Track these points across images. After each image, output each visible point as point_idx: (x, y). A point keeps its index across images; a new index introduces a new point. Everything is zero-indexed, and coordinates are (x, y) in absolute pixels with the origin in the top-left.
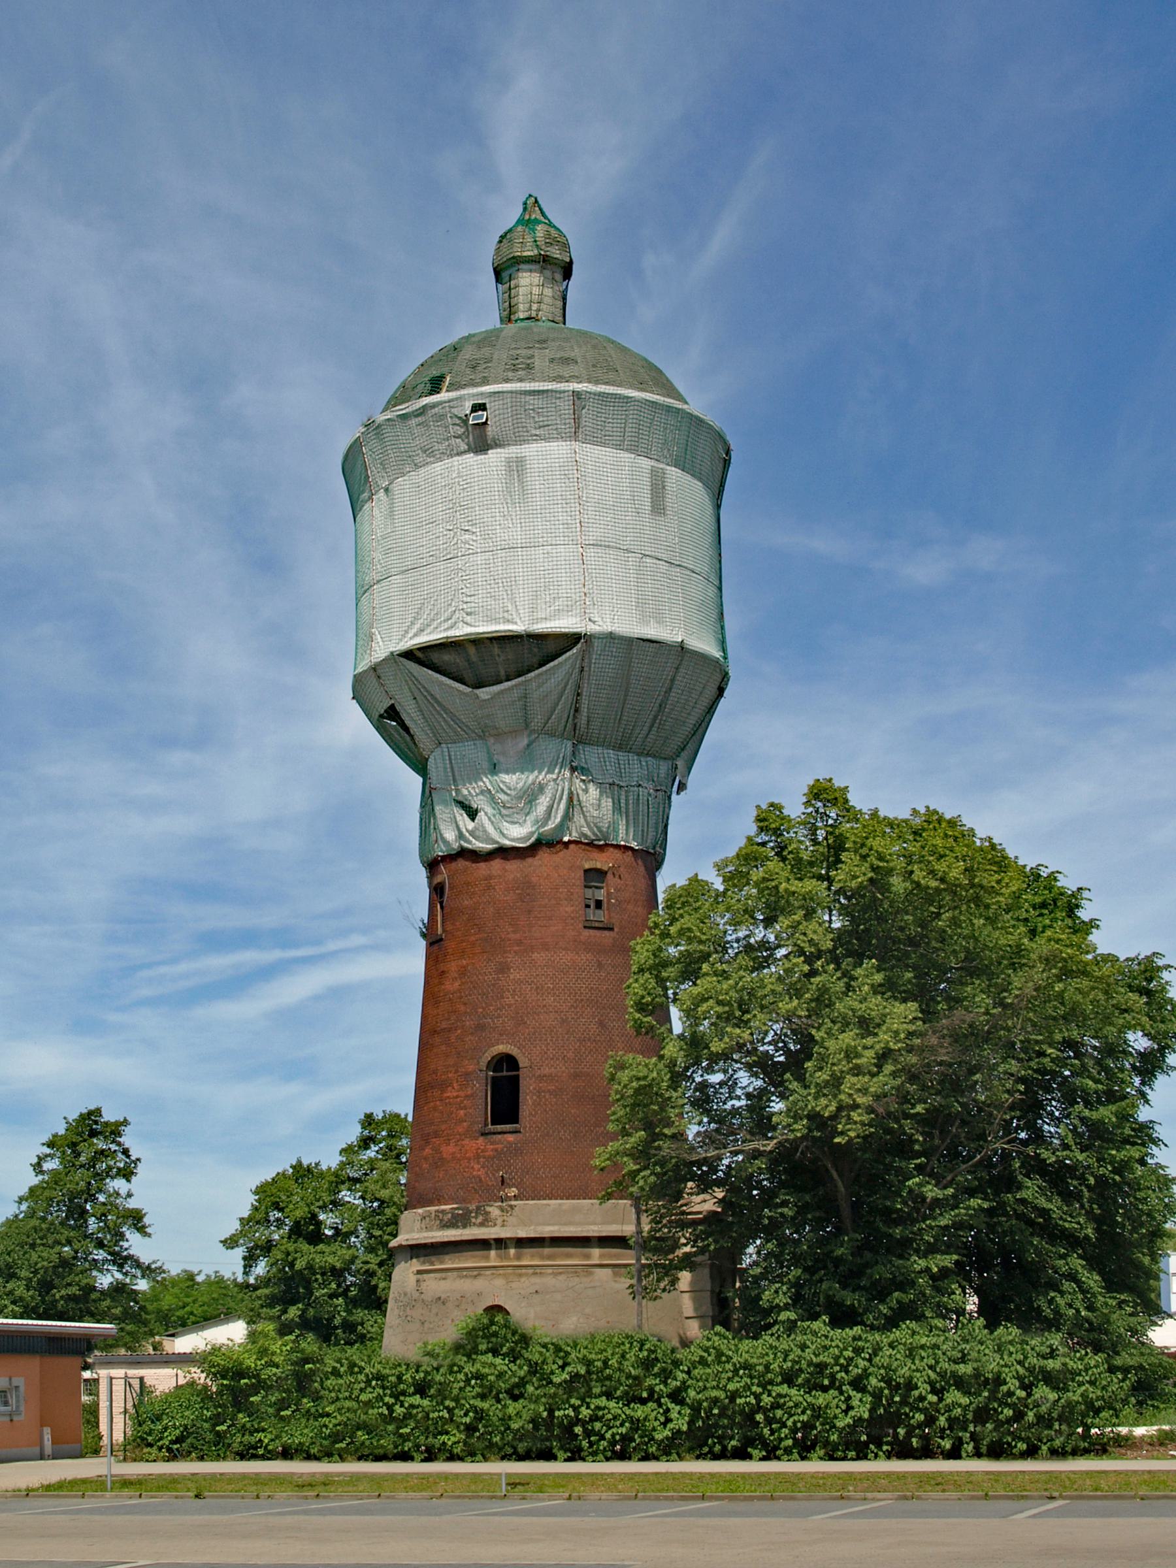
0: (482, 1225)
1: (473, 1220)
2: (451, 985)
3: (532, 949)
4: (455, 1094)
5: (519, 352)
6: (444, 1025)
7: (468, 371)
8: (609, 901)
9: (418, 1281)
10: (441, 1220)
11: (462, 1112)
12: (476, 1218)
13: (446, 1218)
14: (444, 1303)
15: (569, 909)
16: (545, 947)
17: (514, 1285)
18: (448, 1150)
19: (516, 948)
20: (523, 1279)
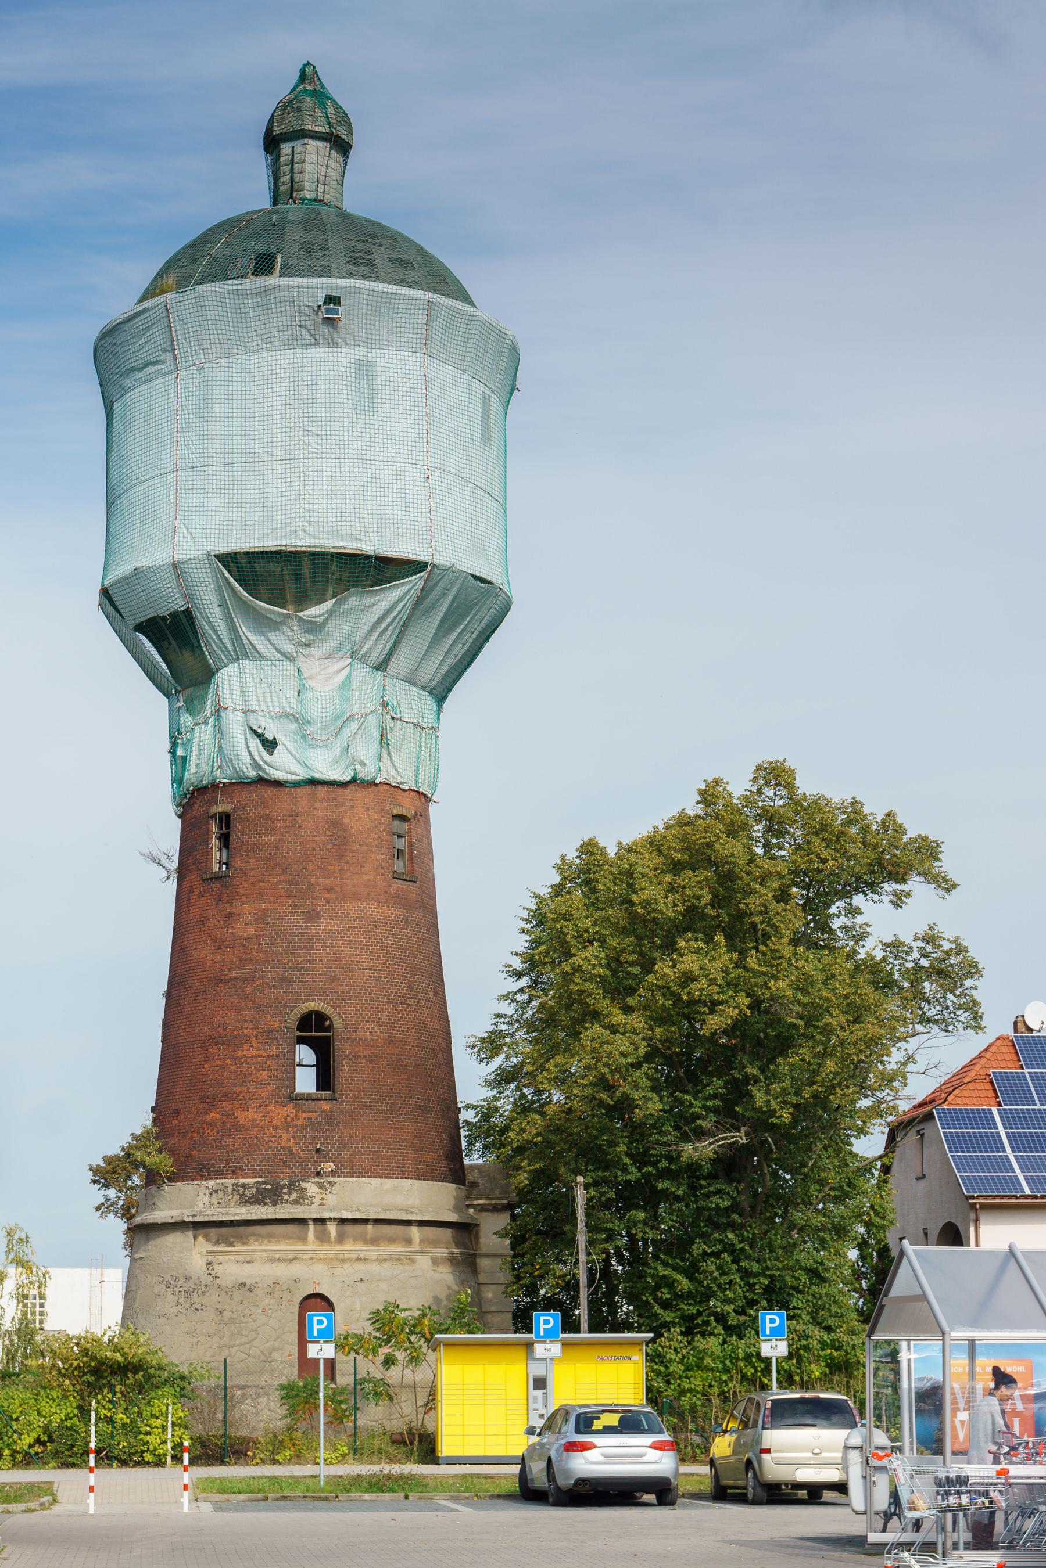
0: (296, 1202)
1: (286, 1197)
3: (344, 898)
4: (254, 1053)
6: (233, 974)
9: (209, 1264)
11: (265, 1074)
12: (289, 1194)
13: (248, 1193)
14: (250, 1290)
15: (380, 857)
16: (357, 897)
18: (244, 1117)
20: (346, 1265)
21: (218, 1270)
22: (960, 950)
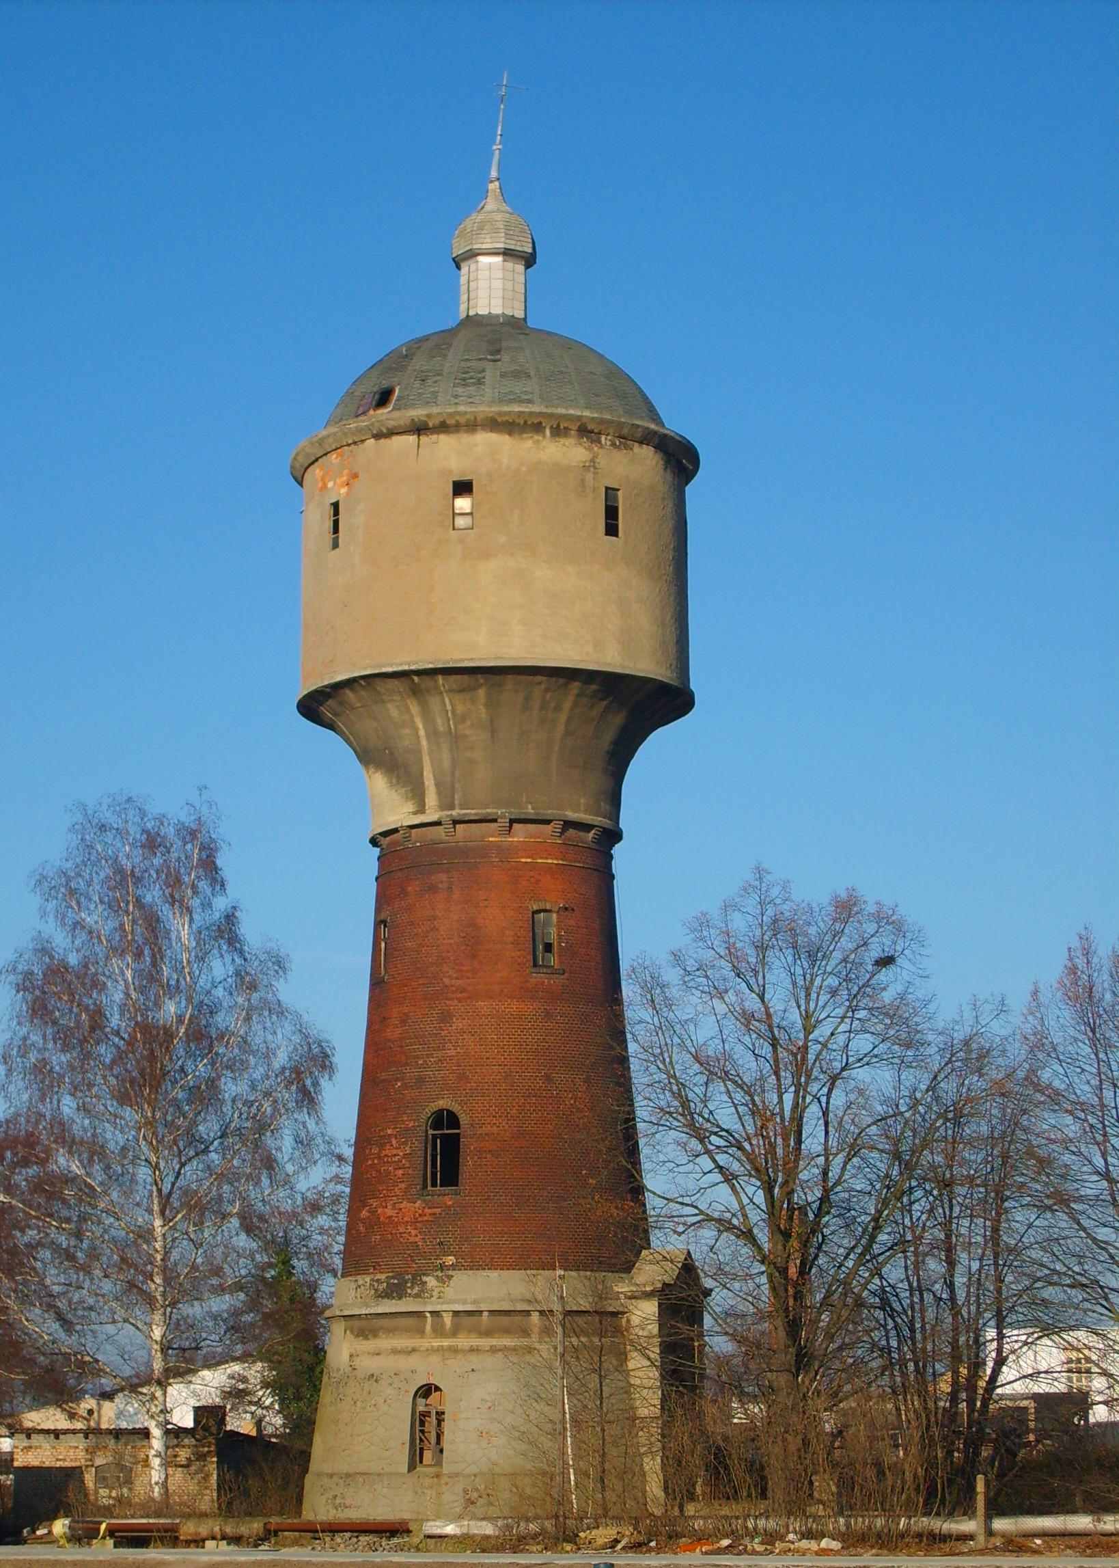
0: (417, 1296)
2: (393, 1032)
5: (469, 364)
7: (417, 384)
8: (559, 943)
10: (376, 1290)
12: (412, 1288)
14: (376, 1381)
17: (448, 1362)
19: (459, 995)
21: (357, 1362)
22: (703, 922)
